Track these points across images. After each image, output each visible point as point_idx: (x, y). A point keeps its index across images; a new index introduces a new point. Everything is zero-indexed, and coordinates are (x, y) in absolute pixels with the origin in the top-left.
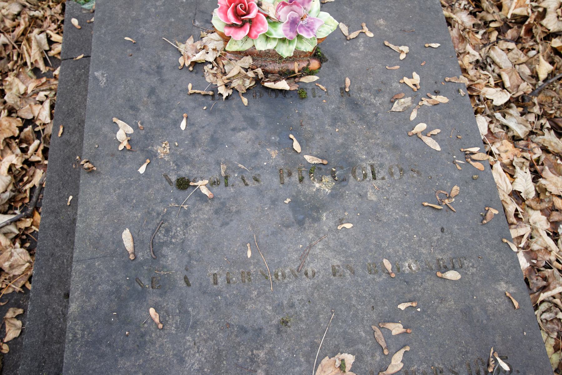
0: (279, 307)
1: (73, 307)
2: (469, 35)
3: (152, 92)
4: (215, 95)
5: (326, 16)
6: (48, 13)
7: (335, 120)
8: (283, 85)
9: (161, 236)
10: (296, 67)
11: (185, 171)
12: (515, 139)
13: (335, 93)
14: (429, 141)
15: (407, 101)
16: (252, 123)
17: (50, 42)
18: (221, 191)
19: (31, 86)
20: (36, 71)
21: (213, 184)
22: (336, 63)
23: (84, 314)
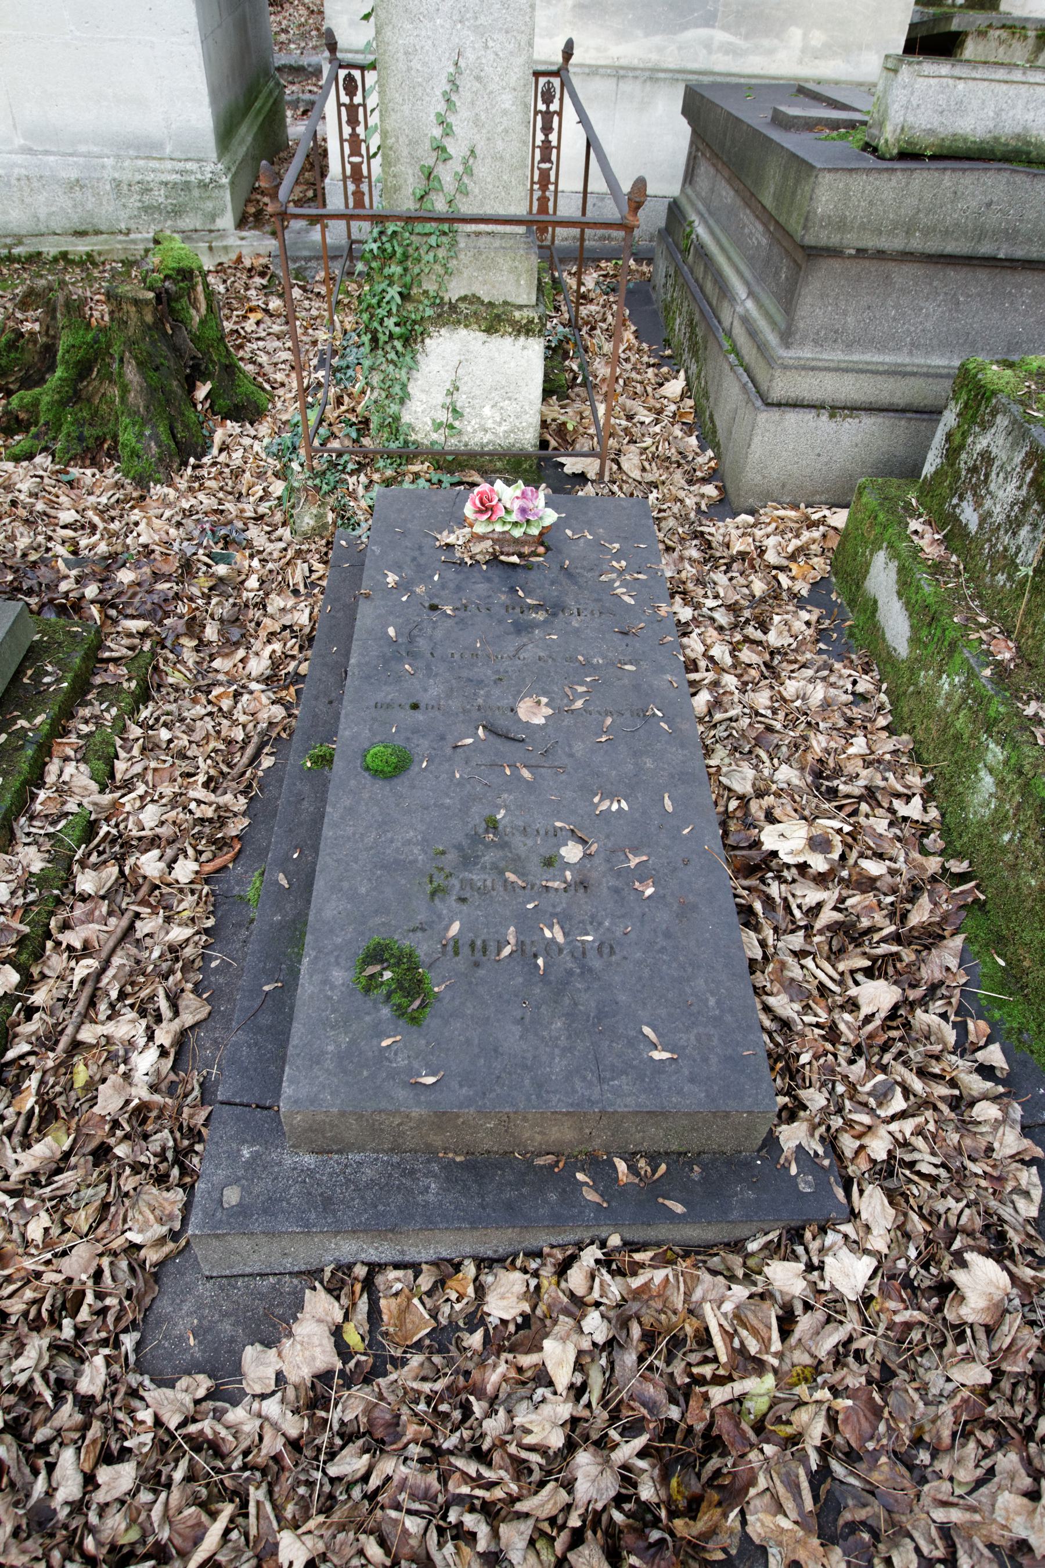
0: (498, 672)
1: (352, 661)
2: (883, 729)
3: (414, 559)
4: (463, 563)
5: (549, 511)
6: (313, 547)
7: (553, 583)
8: (515, 559)
9: (416, 632)
10: (526, 550)
11: (436, 601)
12: (720, 629)
13: (555, 567)
14: (626, 598)
15: (614, 576)
16: (489, 580)
17: (311, 571)
18: (461, 614)
19: (290, 603)
20: (296, 592)
21: (454, 610)
22: (560, 552)
23: (359, 665)
